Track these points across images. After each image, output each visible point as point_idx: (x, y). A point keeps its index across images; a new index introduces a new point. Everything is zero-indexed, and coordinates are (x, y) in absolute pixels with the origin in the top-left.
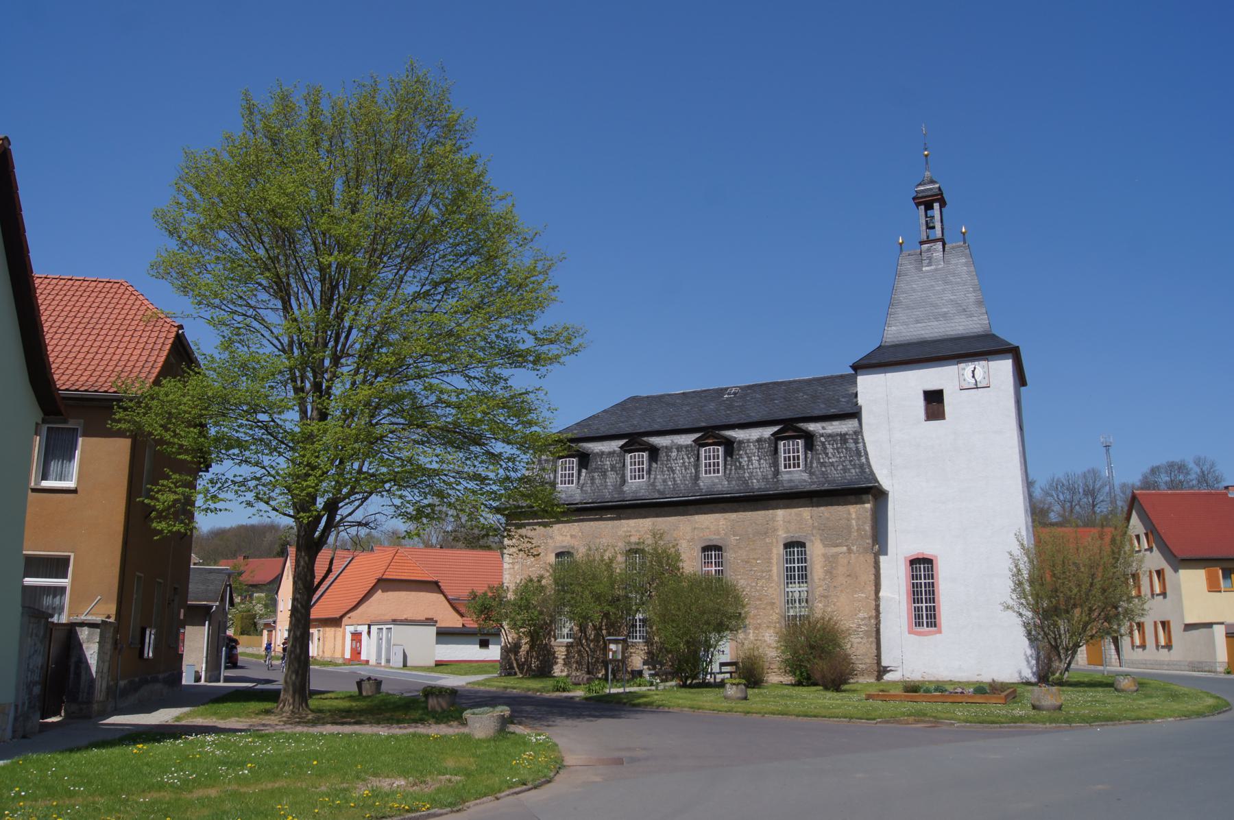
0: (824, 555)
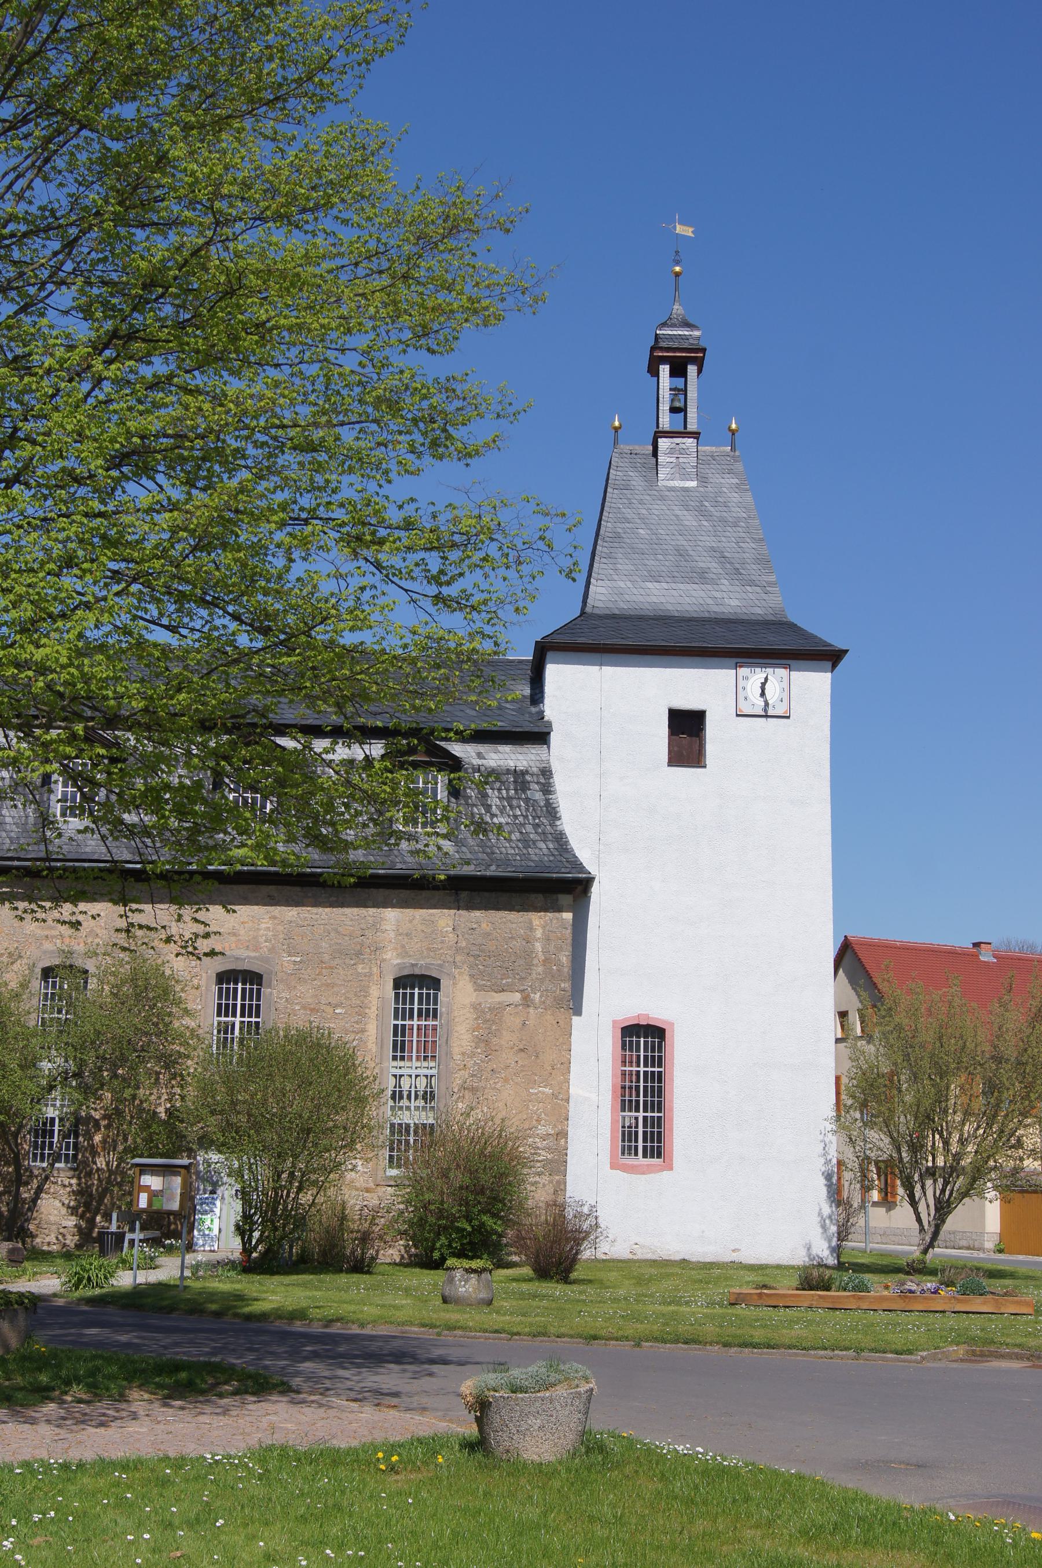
0: (476, 1007)
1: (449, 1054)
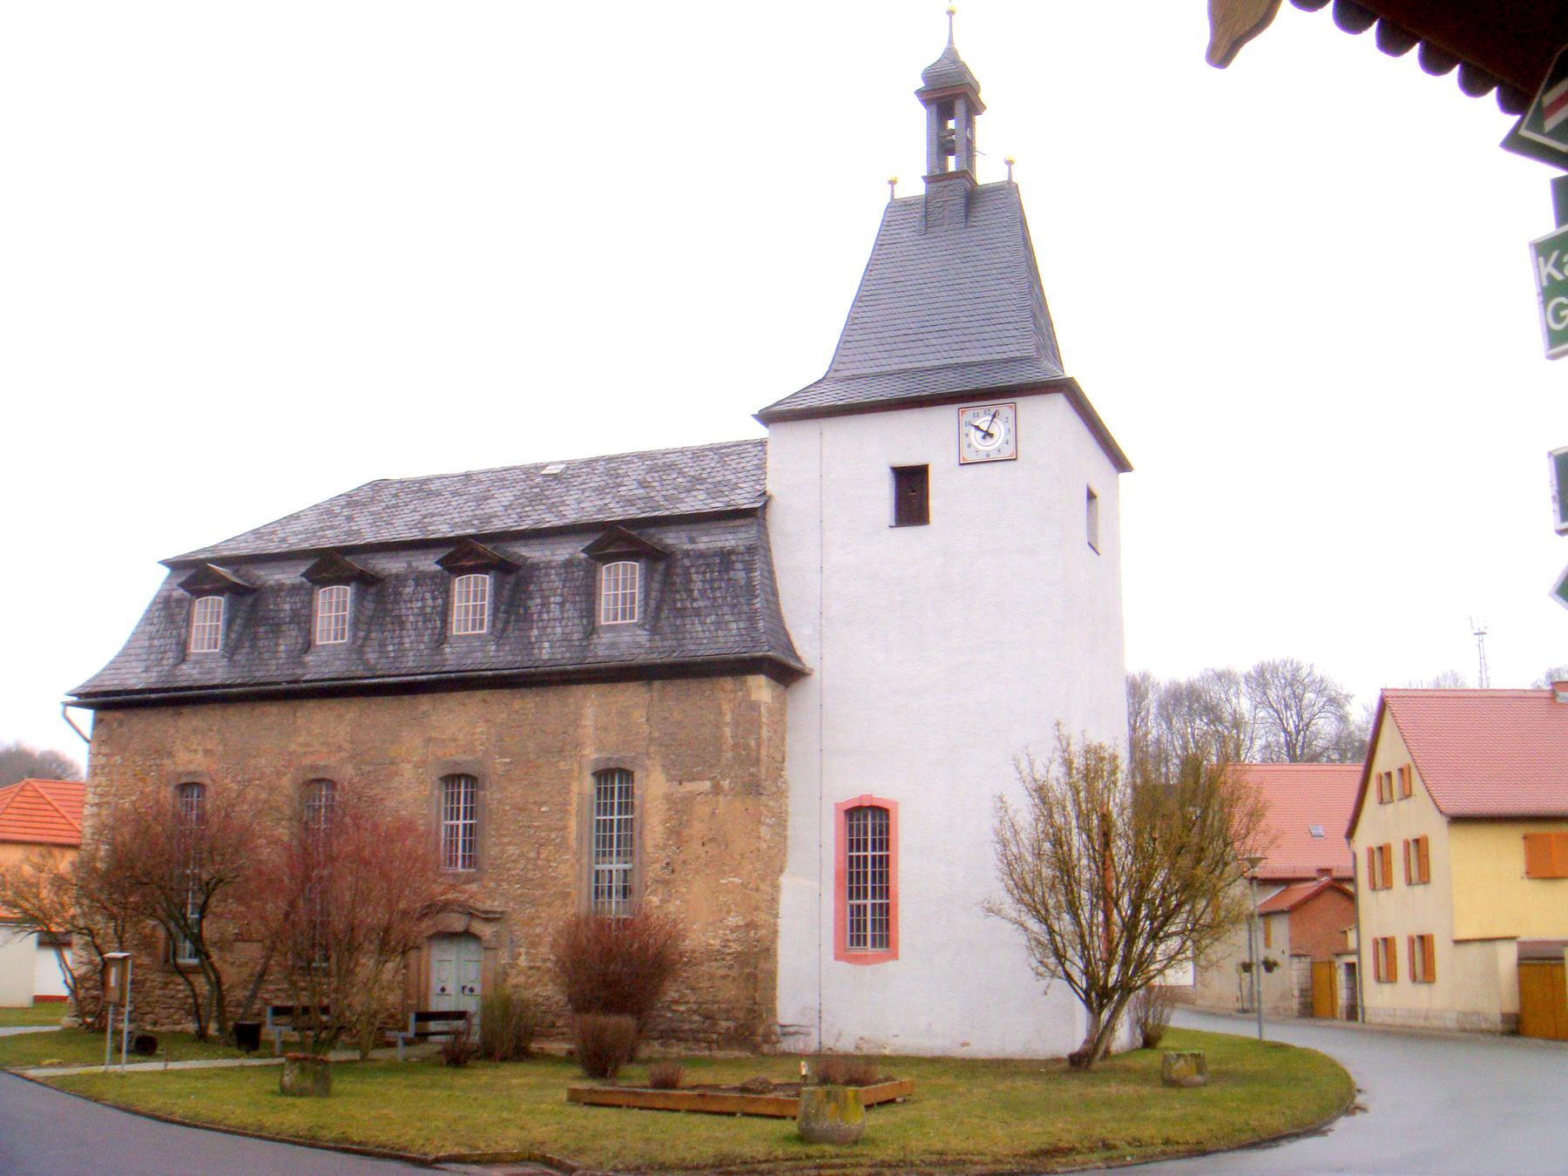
1: (643, 846)
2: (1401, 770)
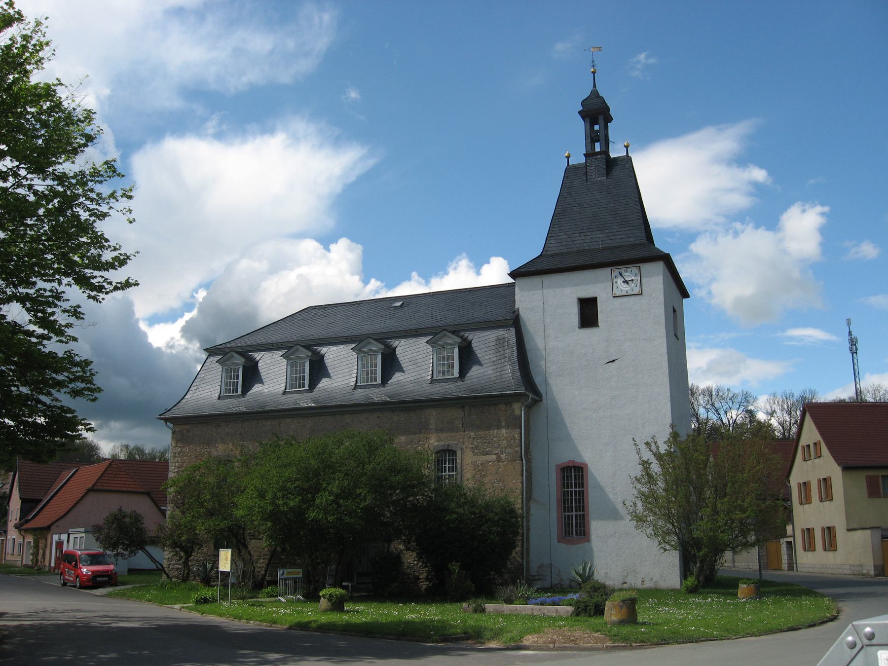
2: (815, 444)
